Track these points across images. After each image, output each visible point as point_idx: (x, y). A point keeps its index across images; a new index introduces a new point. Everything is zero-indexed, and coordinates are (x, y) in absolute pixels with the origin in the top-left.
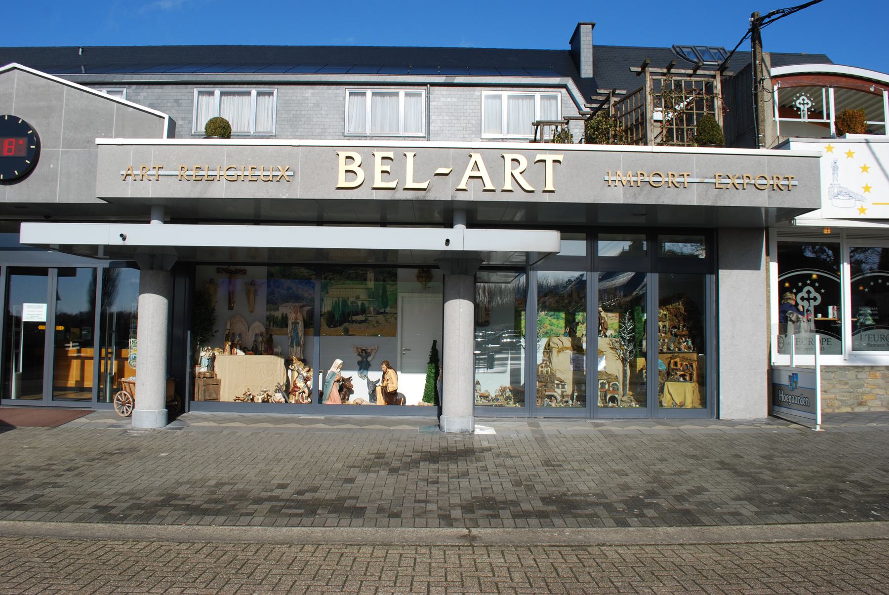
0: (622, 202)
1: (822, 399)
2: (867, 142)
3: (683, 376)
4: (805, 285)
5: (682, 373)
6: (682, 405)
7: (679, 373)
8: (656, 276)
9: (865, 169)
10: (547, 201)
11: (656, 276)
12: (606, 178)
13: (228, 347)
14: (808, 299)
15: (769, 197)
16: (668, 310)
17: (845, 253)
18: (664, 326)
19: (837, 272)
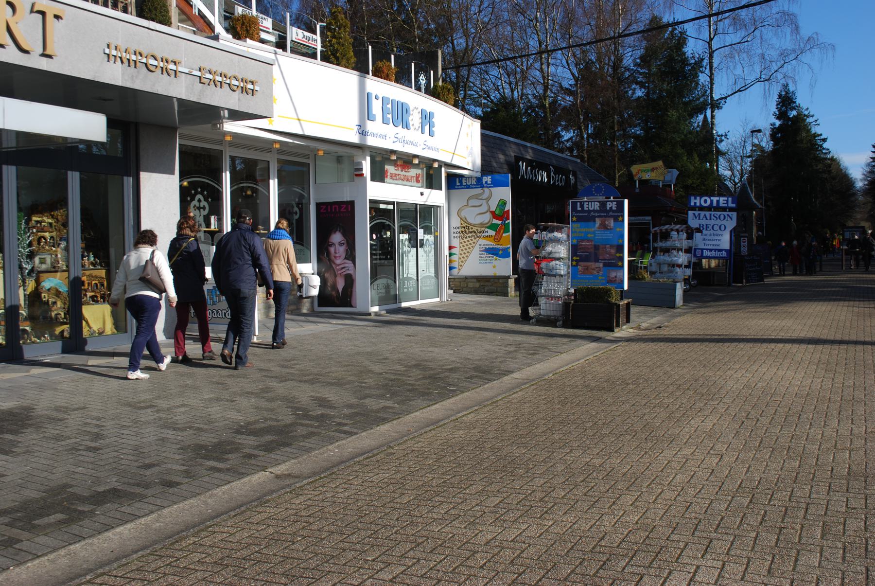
0: (120, 84)
1: (629, 224)
2: (276, 53)
3: (92, 297)
4: (197, 193)
5: (93, 294)
6: (101, 333)
7: (89, 294)
8: (77, 175)
9: (57, 17)
10: (45, 69)
11: (77, 175)
12: (107, 51)
13: (853, 199)
14: (199, 208)
15: (239, 99)
16: (53, 217)
17: (226, 163)
18: (52, 237)
19: (219, 181)
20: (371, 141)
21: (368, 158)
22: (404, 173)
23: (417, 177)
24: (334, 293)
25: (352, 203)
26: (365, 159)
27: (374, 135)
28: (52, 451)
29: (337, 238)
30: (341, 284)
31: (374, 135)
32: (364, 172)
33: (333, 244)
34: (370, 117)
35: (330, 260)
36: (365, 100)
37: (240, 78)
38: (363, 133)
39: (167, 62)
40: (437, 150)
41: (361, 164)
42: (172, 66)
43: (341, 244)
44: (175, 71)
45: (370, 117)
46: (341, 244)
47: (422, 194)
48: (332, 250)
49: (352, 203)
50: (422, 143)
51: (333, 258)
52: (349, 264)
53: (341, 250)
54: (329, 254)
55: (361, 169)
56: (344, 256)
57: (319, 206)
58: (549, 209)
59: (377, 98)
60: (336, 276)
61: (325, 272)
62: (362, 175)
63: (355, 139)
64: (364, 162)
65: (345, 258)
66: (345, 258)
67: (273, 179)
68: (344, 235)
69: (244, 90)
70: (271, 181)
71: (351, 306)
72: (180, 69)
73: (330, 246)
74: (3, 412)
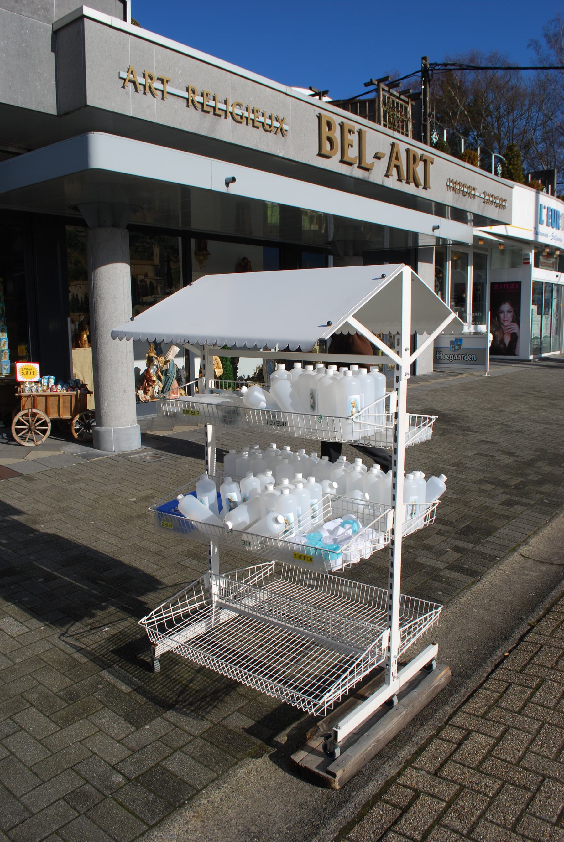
15: (498, 213)
17: (449, 255)
20: (542, 240)
21: (533, 251)
22: (547, 261)
23: (553, 264)
24: (502, 346)
25: (519, 283)
26: (531, 252)
27: (542, 235)
28: (172, 476)
29: (506, 307)
30: (507, 340)
31: (542, 235)
32: (530, 261)
33: (503, 312)
34: (541, 222)
35: (500, 323)
36: (539, 208)
37: (455, 181)
38: (536, 233)
39: (151, 78)
40: (560, 240)
41: (528, 255)
42: (157, 85)
43: (509, 312)
44: (163, 92)
45: (541, 222)
46: (509, 312)
47: (557, 276)
48: (502, 315)
49: (519, 283)
50: (550, 234)
51: (502, 321)
52: (515, 325)
53: (509, 316)
54: (499, 318)
55: (529, 259)
56: (511, 320)
57: (493, 285)
58: (481, 243)
59: (544, 208)
60: (504, 334)
61: (495, 331)
62: (529, 263)
63: (530, 236)
64: (530, 254)
65: (512, 322)
66: (512, 322)
67: (470, 266)
68: (512, 305)
69: (498, 205)
70: (469, 267)
71: (515, 355)
72: (169, 89)
73: (501, 313)
74: (552, 507)
